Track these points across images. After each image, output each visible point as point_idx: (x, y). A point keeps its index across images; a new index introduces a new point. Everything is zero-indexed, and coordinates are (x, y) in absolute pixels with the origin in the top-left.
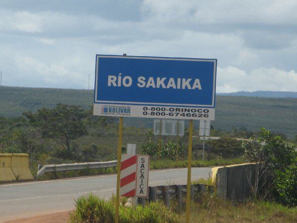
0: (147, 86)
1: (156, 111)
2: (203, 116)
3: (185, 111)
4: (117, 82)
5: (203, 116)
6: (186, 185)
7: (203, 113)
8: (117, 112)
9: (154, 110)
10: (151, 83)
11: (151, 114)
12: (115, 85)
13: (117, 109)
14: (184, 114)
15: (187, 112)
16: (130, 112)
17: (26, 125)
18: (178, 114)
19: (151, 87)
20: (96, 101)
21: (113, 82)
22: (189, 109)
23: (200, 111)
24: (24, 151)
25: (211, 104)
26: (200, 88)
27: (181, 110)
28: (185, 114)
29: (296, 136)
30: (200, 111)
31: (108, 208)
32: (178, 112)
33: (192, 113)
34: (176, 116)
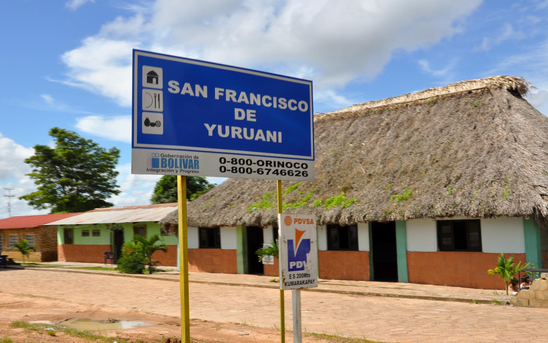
0: (257, 139)
1: (238, 166)
2: (301, 174)
3: (279, 166)
4: (242, 134)
5: (301, 174)
6: (524, 254)
7: (301, 170)
8: (176, 167)
9: (236, 163)
10: (260, 135)
11: (232, 171)
12: (240, 137)
13: (176, 160)
14: (277, 170)
15: (280, 168)
16: (198, 168)
17: (330, 182)
18: (270, 170)
19: (260, 140)
20: (312, 158)
21: (238, 134)
22: (267, 166)
23: (297, 166)
24: (115, 263)
25: (138, 142)
26: (207, 125)
27: (273, 164)
28: (279, 172)
29: (180, 341)
30: (297, 166)
31: (509, 87)
32: (269, 167)
33: (287, 169)
34: (268, 174)
